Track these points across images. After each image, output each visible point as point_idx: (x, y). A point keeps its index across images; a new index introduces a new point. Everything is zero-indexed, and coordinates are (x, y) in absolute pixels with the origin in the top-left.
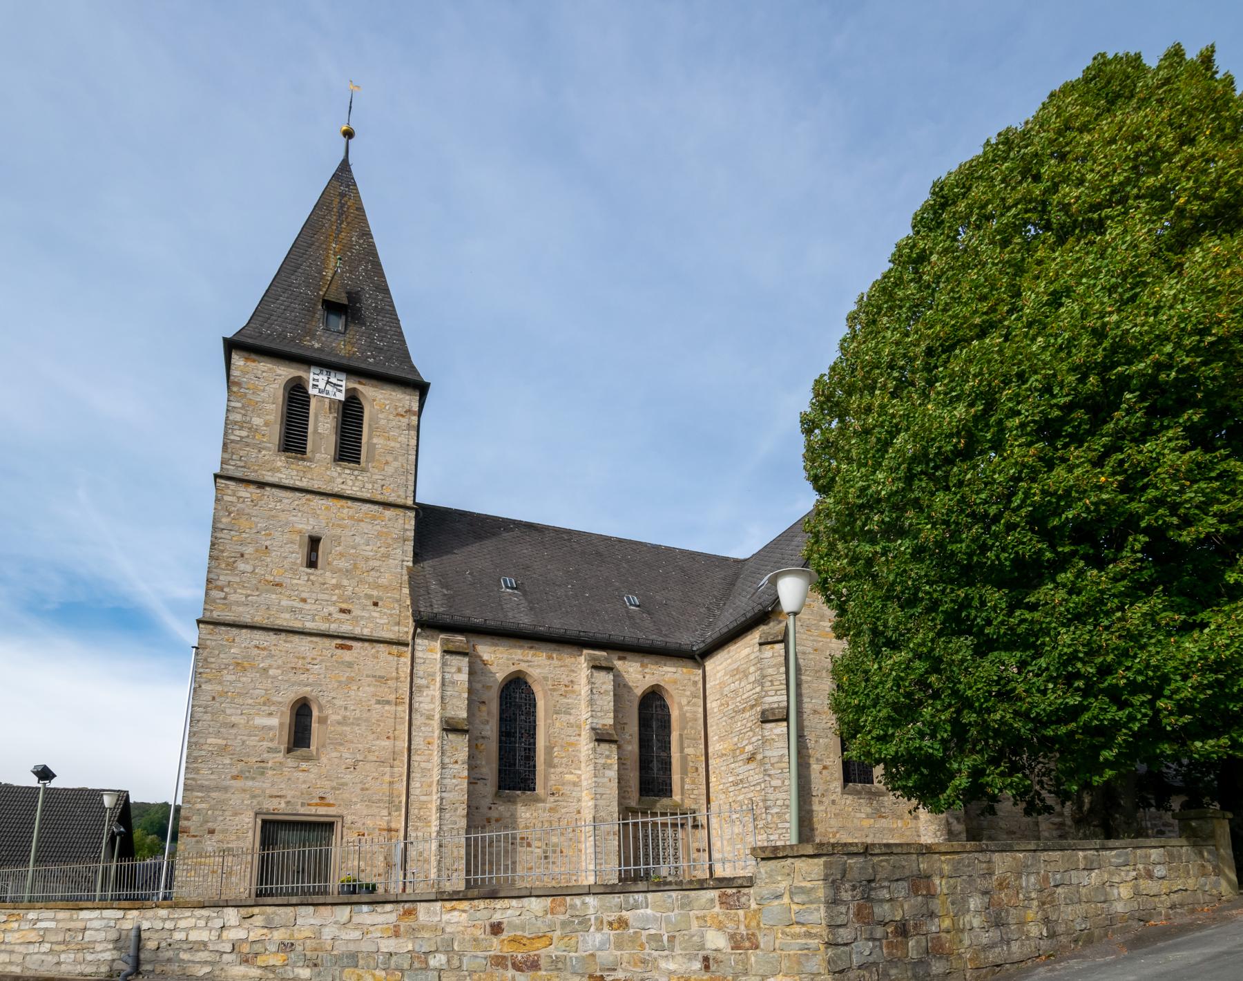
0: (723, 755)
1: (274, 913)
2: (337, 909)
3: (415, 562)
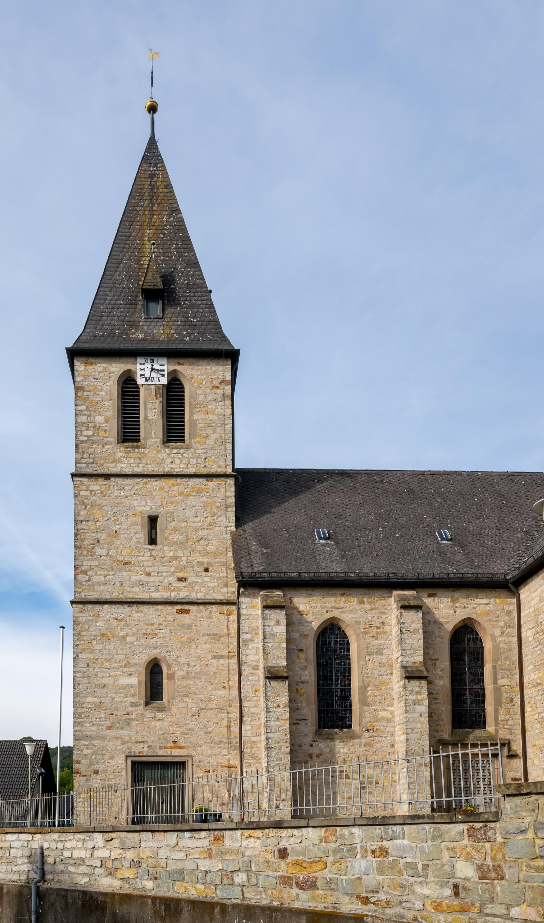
1: (126, 837)
2: (168, 835)
3: (237, 527)
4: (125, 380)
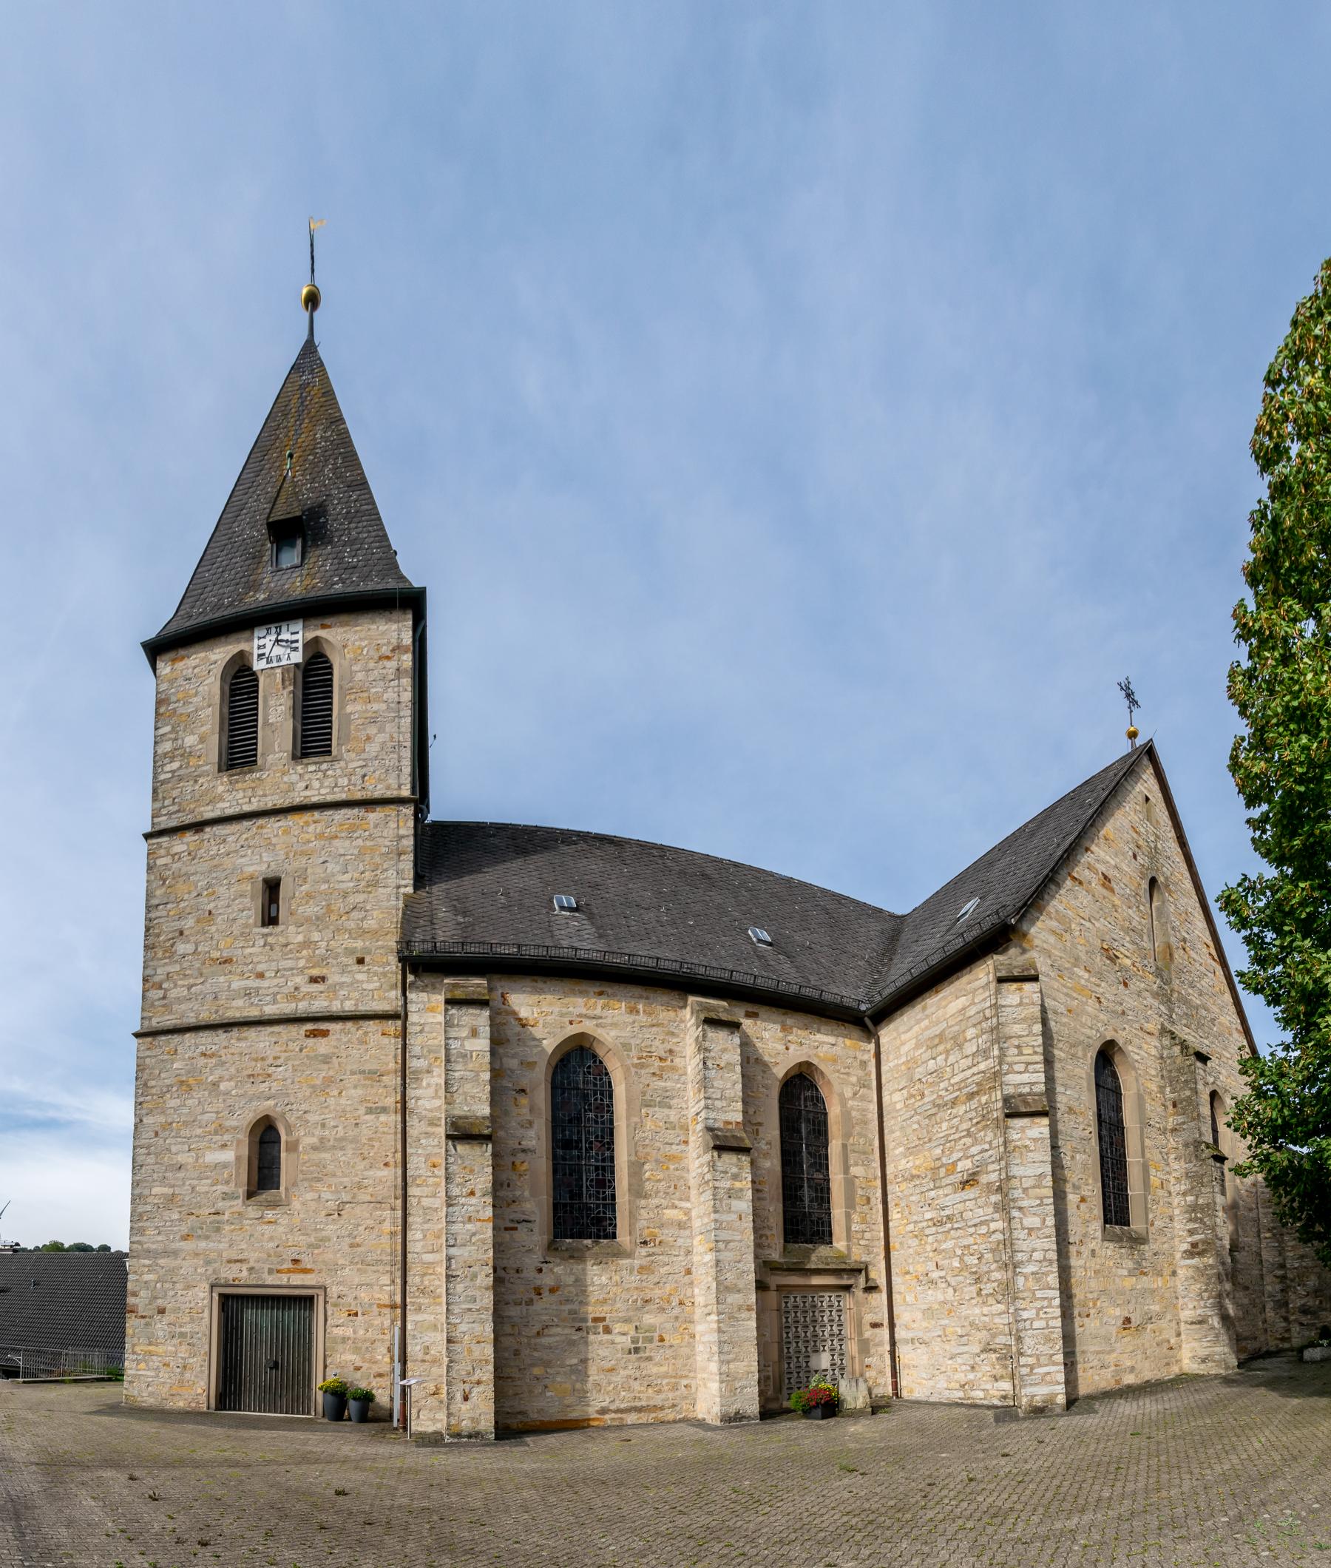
0: (913, 1177)
3: (416, 887)
4: (239, 671)
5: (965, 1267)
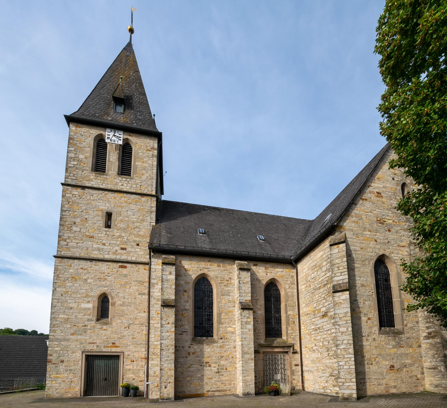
0: (308, 314)
3: (156, 223)
4: (100, 140)
5: (324, 345)
